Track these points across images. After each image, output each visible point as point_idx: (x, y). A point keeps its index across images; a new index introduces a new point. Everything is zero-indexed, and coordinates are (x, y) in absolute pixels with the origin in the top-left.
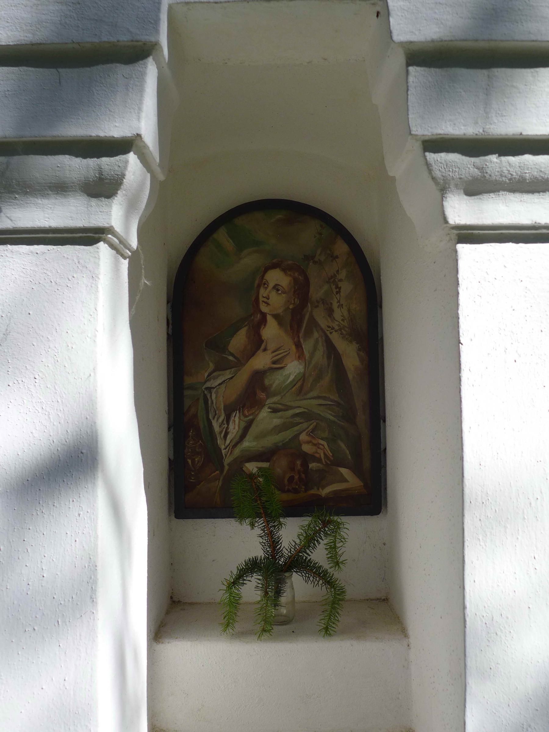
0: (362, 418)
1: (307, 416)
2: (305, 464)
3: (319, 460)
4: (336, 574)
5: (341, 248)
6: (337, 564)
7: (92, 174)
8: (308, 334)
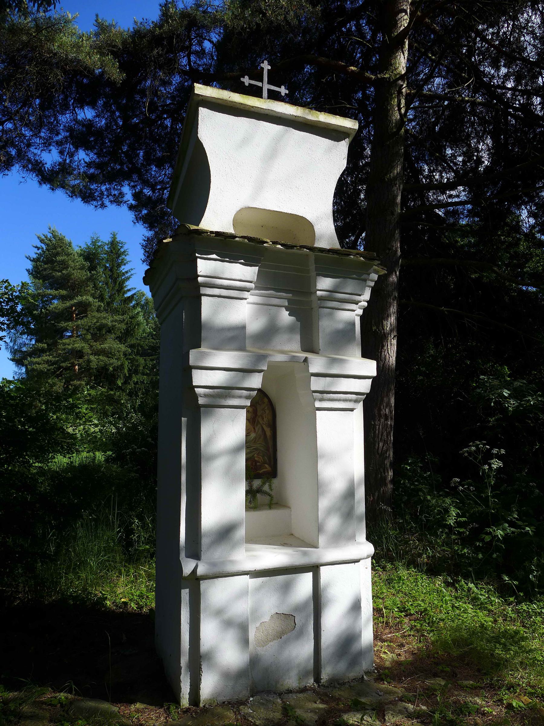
0: (271, 450)
1: (256, 449)
2: (256, 463)
3: (259, 462)
4: (271, 493)
5: (266, 400)
6: (272, 490)
7: (248, 395)
8: (257, 425)
